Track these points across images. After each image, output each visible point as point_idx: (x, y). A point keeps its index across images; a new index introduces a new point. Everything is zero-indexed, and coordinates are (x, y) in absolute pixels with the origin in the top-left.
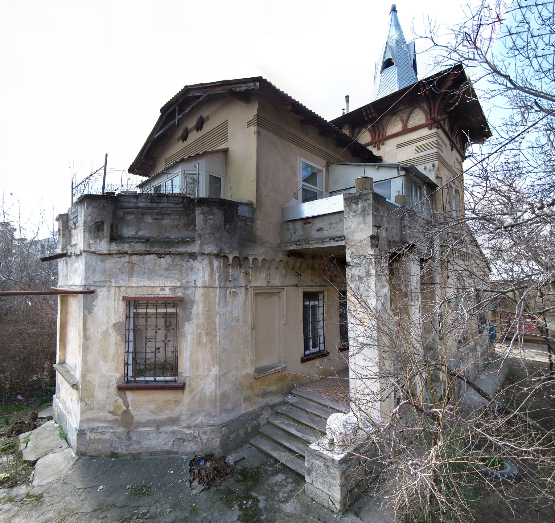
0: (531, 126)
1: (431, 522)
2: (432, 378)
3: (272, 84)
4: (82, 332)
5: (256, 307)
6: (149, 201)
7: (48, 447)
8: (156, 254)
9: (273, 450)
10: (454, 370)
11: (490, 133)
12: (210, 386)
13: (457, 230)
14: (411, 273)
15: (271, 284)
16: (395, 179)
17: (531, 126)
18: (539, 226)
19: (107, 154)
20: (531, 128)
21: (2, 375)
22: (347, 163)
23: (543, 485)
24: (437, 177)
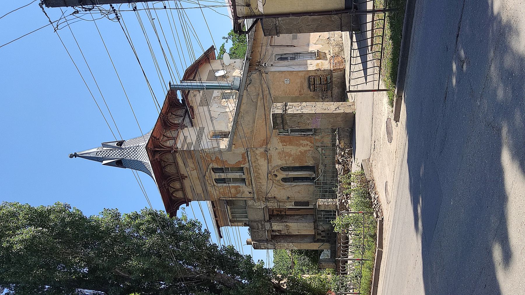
0: (323, 227)
1: (1, 214)
2: (159, 140)
3: (87, 214)
4: (407, 153)
5: (173, 157)
6: (329, 92)
7: (180, 196)
8: (239, 88)
9: (147, 164)
10: (329, 276)
11: (346, 114)
12: (269, 44)
13: (227, 192)
14: (329, 68)
15: (277, 27)
16: (206, 220)
17: (323, 227)
18: (103, 10)
19: (71, 156)
20: (305, 215)
21: (524, 224)
22: (412, 197)
23: (182, 231)
24: (215, 98)
